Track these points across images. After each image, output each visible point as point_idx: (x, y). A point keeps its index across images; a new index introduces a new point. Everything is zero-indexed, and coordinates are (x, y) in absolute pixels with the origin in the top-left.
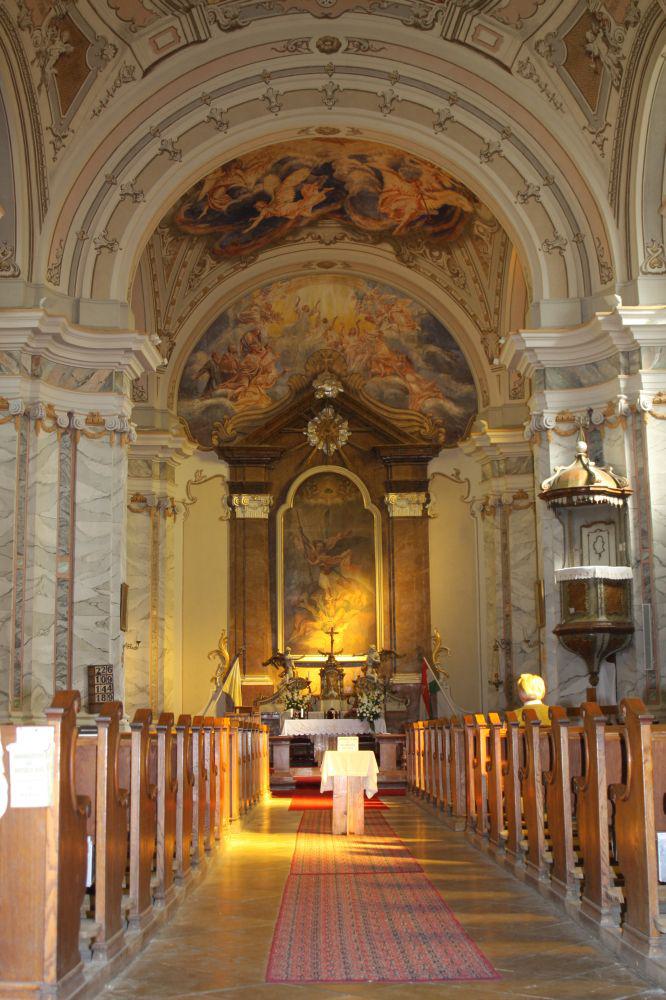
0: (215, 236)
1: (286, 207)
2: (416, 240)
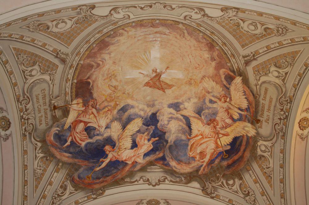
0: (74, 167)
2: (216, 175)
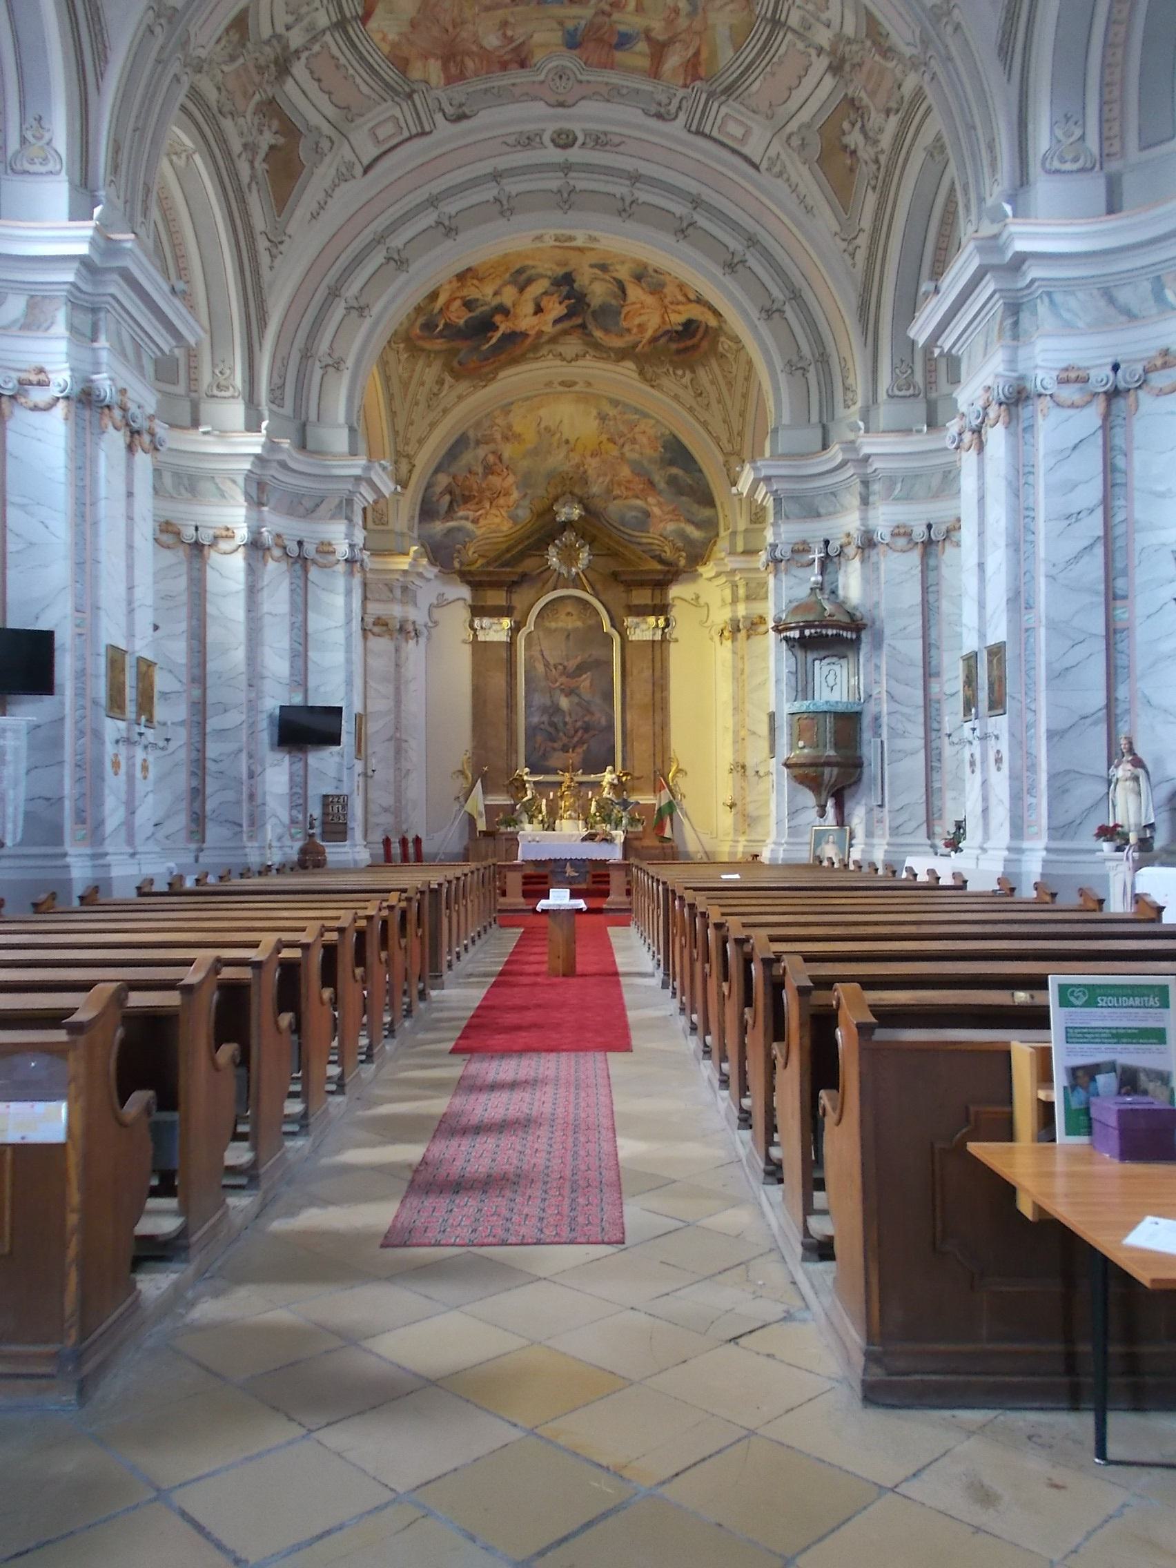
0: (453, 353)
1: (526, 321)
